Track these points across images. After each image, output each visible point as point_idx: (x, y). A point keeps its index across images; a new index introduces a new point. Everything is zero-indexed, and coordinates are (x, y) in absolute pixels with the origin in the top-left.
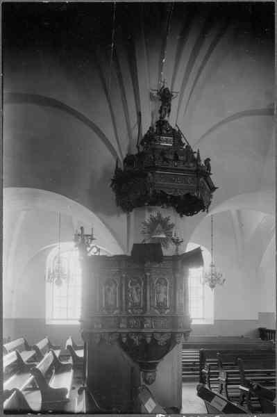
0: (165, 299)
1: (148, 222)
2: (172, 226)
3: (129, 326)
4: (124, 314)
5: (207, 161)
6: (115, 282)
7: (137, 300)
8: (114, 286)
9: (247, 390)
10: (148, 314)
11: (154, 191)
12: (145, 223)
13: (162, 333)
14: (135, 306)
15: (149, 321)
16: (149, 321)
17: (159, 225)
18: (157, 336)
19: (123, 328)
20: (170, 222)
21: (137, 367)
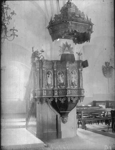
0: (75, 81)
1: (62, 46)
2: (72, 48)
3: (58, 94)
4: (56, 88)
5: (90, 19)
6: (51, 73)
7: (62, 81)
8: (50, 74)
9: (61, 112)
10: (69, 87)
11: (72, 30)
12: (60, 47)
13: (74, 97)
14: (62, 84)
15: (69, 91)
16: (69, 91)
17: (67, 47)
18: (72, 99)
19: (56, 95)
20: (71, 46)
21: (59, 115)
